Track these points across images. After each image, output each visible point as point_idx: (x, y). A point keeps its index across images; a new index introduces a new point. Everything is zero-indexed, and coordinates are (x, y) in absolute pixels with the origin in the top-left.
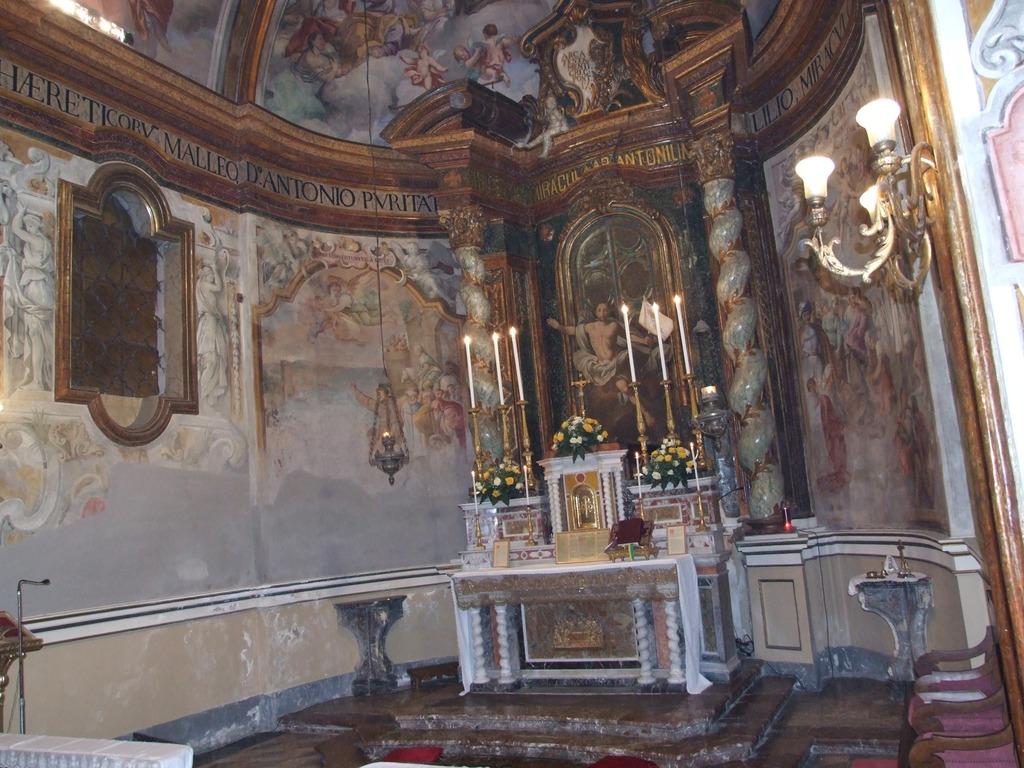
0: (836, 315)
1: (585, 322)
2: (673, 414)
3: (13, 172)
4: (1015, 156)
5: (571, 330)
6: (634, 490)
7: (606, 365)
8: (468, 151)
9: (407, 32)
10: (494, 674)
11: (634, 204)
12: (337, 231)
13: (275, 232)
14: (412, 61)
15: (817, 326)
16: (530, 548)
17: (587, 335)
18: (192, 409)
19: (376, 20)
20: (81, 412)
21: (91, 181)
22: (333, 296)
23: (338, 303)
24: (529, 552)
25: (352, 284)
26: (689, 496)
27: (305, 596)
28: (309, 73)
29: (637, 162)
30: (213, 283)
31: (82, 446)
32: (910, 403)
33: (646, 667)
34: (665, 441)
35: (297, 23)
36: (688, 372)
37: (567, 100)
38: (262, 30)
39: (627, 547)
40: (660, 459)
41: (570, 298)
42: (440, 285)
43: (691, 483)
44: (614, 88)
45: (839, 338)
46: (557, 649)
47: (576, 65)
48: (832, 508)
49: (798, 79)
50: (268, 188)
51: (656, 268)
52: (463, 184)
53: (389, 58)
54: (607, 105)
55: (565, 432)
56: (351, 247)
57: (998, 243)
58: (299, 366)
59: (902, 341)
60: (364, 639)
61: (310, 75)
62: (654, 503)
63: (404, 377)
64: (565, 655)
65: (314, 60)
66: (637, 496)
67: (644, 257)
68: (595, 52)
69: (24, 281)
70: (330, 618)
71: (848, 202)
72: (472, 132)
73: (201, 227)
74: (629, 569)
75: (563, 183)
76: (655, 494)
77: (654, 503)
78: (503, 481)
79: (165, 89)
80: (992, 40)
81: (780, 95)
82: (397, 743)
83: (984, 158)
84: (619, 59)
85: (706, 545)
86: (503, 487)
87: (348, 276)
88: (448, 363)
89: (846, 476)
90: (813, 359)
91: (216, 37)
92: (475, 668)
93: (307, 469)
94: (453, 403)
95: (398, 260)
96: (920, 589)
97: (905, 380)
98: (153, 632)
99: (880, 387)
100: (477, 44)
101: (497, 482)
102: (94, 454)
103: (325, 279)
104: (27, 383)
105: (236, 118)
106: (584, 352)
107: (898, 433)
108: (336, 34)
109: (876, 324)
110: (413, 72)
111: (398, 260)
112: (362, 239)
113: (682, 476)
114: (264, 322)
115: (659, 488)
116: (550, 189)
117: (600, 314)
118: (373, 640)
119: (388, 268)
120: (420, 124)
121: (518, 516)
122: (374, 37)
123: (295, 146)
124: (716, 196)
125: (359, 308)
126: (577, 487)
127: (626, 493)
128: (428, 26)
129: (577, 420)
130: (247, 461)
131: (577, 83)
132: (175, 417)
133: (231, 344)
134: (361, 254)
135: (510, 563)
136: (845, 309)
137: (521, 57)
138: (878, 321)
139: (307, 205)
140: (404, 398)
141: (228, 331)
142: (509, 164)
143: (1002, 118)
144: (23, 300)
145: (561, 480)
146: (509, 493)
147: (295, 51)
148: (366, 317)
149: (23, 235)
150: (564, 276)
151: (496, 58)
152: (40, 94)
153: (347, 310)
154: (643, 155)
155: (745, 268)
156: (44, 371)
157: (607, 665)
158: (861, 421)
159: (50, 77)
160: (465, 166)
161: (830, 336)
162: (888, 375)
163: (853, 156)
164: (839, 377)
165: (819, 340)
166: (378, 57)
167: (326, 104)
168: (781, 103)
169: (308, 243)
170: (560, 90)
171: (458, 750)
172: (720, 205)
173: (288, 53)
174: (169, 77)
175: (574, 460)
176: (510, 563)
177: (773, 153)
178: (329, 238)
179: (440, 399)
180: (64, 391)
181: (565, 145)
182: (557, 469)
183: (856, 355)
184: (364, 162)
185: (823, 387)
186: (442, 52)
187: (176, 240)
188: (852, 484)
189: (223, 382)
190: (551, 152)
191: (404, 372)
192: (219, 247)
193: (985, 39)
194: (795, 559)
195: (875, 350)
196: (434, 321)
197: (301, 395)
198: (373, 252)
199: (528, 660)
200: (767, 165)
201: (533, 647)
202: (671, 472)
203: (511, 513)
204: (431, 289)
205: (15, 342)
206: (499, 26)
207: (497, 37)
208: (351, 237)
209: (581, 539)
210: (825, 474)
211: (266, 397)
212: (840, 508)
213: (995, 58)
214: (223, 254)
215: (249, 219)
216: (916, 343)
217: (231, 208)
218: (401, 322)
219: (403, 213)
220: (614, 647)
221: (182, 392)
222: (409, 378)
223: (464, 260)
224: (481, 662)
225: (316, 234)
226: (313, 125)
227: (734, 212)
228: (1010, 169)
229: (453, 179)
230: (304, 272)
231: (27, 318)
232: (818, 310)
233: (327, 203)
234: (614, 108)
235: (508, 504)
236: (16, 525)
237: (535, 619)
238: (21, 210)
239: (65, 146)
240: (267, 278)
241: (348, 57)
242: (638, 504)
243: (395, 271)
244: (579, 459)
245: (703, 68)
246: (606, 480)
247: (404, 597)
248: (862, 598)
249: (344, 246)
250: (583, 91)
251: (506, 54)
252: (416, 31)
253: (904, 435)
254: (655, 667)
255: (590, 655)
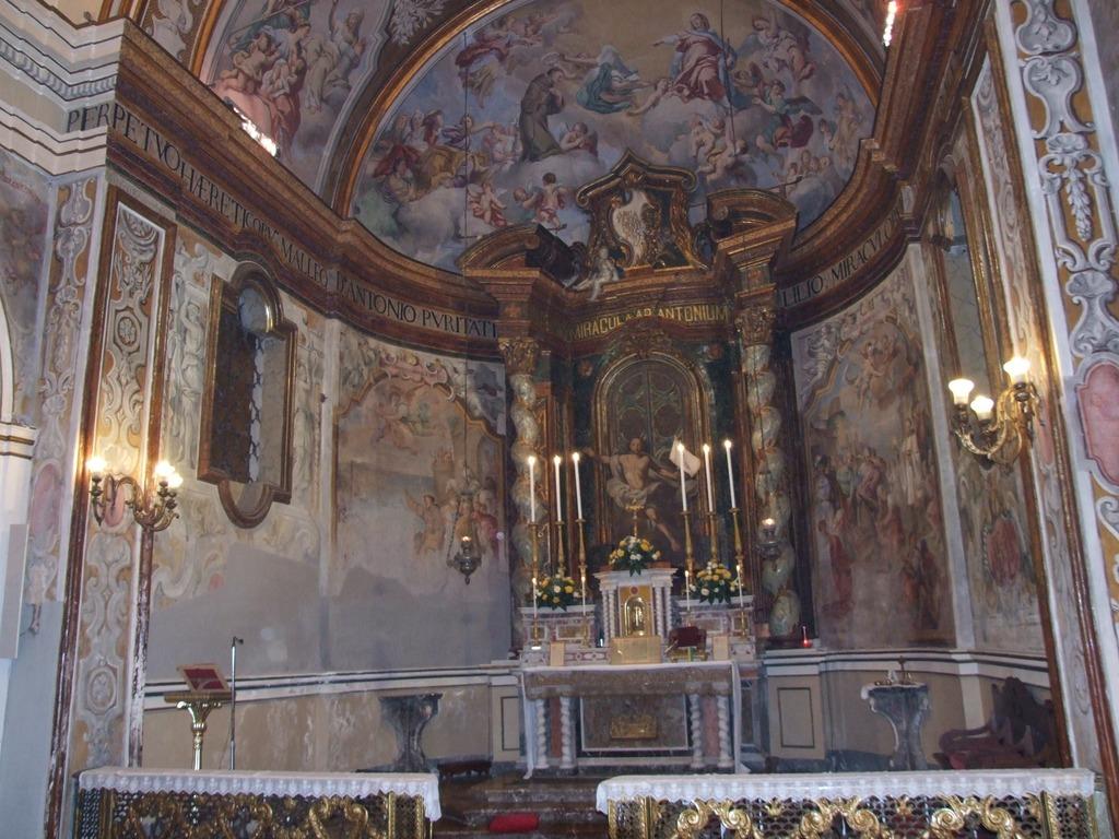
0: (851, 469)
1: (620, 454)
2: (692, 541)
3: (184, 264)
4: (1091, 402)
5: (606, 459)
6: (681, 604)
7: (637, 494)
8: (530, 287)
9: (477, 169)
10: (555, 761)
11: (673, 354)
12: (399, 344)
13: (354, 339)
14: (475, 195)
15: (832, 477)
16: (584, 650)
17: (621, 464)
18: (285, 498)
19: (451, 154)
20: (212, 491)
21: (233, 278)
22: (393, 404)
23: (397, 411)
24: (583, 654)
25: (409, 396)
26: (730, 611)
27: (357, 686)
28: (389, 194)
29: (676, 317)
30: (306, 381)
31: (212, 524)
32: (919, 545)
33: (698, 754)
34: (710, 563)
35: (387, 149)
36: (711, 510)
37: (618, 254)
38: (361, 152)
39: (687, 651)
40: (708, 578)
41: (605, 429)
42: (485, 406)
43: (734, 600)
44: (659, 250)
45: (852, 489)
46: (613, 740)
47: (629, 223)
48: (835, 631)
49: (829, 271)
50: (350, 297)
51: (687, 413)
52: (522, 317)
53: (457, 189)
54: (653, 262)
55: (625, 548)
56: (410, 361)
57: (1081, 448)
58: (363, 467)
59: (915, 496)
60: (404, 732)
61: (390, 196)
62: (699, 616)
63: (448, 487)
64: (620, 746)
65: (396, 183)
66: (685, 609)
67: (677, 402)
68: (647, 215)
69: (184, 366)
70: (373, 711)
71: (870, 378)
72: (538, 273)
73: (302, 328)
74: (689, 668)
75: (605, 325)
76: (701, 608)
77: (699, 616)
78: (563, 588)
79: (294, 201)
80: (1080, 337)
81: (811, 280)
82: (496, 811)
83: (1075, 401)
84: (665, 223)
85: (748, 653)
86: (563, 594)
87: (406, 387)
88: (487, 478)
89: (851, 605)
90: (826, 504)
91: (325, 153)
92: (537, 755)
93: (365, 566)
94: (489, 516)
95: (449, 377)
96: (921, 695)
97: (915, 527)
98: (249, 706)
99: (889, 532)
100: (535, 188)
101: (557, 589)
102: (219, 532)
103: (388, 388)
104: (180, 460)
105: (338, 231)
106: (616, 480)
107: (904, 569)
108: (417, 162)
109: (889, 479)
110: (475, 205)
111: (449, 377)
112: (420, 354)
113: (726, 593)
114: (342, 422)
115: (706, 603)
116: (592, 328)
117: (634, 448)
118: (412, 733)
119: (441, 384)
120: (490, 258)
121: (571, 622)
122: (449, 170)
123: (378, 261)
124: (755, 358)
125: (414, 418)
126: (628, 596)
127: (674, 605)
128: (496, 167)
129: (633, 540)
130: (319, 554)
131: (630, 240)
132: (274, 504)
133: (314, 440)
134: (418, 368)
135: (566, 662)
136: (859, 466)
137: (574, 206)
138: (892, 477)
139: (378, 317)
140: (447, 507)
141: (313, 429)
142: (558, 301)
143: (1084, 380)
144: (183, 382)
145: (616, 592)
146: (567, 600)
147: (382, 174)
148: (419, 427)
149: (187, 324)
150: (601, 409)
151: (551, 203)
152: (205, 196)
153: (404, 420)
154: (682, 311)
155: (778, 422)
156: (192, 450)
157: (658, 754)
158: (868, 559)
159: (214, 180)
160: (525, 300)
161: (843, 486)
162: (898, 519)
163: (879, 343)
164: (849, 522)
165: (832, 489)
166: (448, 188)
167: (399, 224)
168: (811, 287)
169: (377, 353)
170: (614, 244)
171: (552, 817)
172: (759, 368)
173: (375, 175)
174: (300, 191)
175: (631, 574)
176: (566, 662)
177: (800, 327)
178: (393, 350)
179: (479, 512)
180: (206, 472)
181: (611, 293)
182: (609, 582)
183: (867, 503)
184: (430, 283)
185: (833, 526)
186: (503, 191)
187: (283, 339)
188: (855, 612)
189: (307, 478)
190: (598, 298)
191: (448, 484)
192: (311, 349)
193: (1076, 335)
194: (814, 670)
195: (886, 502)
196: (478, 438)
197: (364, 496)
198: (428, 367)
199: (584, 749)
200: (794, 336)
201: (589, 738)
202: (717, 590)
203: (566, 619)
204: (476, 408)
205: (175, 420)
206: (559, 175)
207: (554, 185)
208: (411, 351)
209: (634, 644)
210: (829, 602)
211: (339, 493)
212: (843, 631)
213: (1081, 347)
214: (314, 355)
215: (335, 325)
216: (933, 494)
217: (321, 312)
218: (448, 435)
219: (455, 333)
220: (665, 737)
221: (279, 483)
222: (452, 489)
223: (519, 386)
224: (543, 749)
225: (383, 345)
226: (387, 240)
227: (769, 374)
228: (1088, 408)
229: (513, 311)
230: (372, 380)
231: (184, 399)
232: (833, 463)
233: (393, 317)
234: (658, 266)
235: (565, 609)
236: (165, 592)
237: (593, 712)
238: (187, 299)
239: (218, 244)
240: (344, 383)
241: (423, 183)
242: (684, 616)
243: (446, 387)
244: (635, 574)
245: (755, 250)
246: (611, 597)
247: (440, 696)
248: (872, 702)
249: (404, 359)
250: (635, 248)
251: (560, 201)
252: (483, 169)
253: (910, 571)
254: (704, 755)
255: (644, 745)
